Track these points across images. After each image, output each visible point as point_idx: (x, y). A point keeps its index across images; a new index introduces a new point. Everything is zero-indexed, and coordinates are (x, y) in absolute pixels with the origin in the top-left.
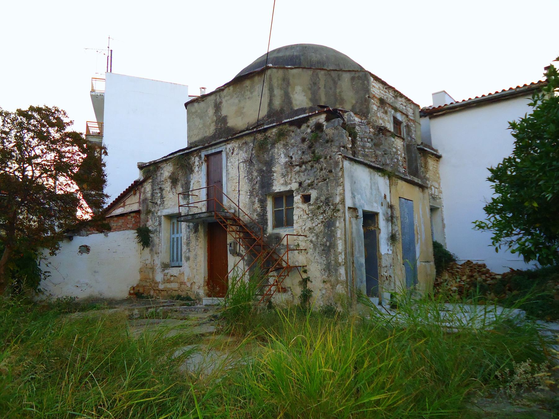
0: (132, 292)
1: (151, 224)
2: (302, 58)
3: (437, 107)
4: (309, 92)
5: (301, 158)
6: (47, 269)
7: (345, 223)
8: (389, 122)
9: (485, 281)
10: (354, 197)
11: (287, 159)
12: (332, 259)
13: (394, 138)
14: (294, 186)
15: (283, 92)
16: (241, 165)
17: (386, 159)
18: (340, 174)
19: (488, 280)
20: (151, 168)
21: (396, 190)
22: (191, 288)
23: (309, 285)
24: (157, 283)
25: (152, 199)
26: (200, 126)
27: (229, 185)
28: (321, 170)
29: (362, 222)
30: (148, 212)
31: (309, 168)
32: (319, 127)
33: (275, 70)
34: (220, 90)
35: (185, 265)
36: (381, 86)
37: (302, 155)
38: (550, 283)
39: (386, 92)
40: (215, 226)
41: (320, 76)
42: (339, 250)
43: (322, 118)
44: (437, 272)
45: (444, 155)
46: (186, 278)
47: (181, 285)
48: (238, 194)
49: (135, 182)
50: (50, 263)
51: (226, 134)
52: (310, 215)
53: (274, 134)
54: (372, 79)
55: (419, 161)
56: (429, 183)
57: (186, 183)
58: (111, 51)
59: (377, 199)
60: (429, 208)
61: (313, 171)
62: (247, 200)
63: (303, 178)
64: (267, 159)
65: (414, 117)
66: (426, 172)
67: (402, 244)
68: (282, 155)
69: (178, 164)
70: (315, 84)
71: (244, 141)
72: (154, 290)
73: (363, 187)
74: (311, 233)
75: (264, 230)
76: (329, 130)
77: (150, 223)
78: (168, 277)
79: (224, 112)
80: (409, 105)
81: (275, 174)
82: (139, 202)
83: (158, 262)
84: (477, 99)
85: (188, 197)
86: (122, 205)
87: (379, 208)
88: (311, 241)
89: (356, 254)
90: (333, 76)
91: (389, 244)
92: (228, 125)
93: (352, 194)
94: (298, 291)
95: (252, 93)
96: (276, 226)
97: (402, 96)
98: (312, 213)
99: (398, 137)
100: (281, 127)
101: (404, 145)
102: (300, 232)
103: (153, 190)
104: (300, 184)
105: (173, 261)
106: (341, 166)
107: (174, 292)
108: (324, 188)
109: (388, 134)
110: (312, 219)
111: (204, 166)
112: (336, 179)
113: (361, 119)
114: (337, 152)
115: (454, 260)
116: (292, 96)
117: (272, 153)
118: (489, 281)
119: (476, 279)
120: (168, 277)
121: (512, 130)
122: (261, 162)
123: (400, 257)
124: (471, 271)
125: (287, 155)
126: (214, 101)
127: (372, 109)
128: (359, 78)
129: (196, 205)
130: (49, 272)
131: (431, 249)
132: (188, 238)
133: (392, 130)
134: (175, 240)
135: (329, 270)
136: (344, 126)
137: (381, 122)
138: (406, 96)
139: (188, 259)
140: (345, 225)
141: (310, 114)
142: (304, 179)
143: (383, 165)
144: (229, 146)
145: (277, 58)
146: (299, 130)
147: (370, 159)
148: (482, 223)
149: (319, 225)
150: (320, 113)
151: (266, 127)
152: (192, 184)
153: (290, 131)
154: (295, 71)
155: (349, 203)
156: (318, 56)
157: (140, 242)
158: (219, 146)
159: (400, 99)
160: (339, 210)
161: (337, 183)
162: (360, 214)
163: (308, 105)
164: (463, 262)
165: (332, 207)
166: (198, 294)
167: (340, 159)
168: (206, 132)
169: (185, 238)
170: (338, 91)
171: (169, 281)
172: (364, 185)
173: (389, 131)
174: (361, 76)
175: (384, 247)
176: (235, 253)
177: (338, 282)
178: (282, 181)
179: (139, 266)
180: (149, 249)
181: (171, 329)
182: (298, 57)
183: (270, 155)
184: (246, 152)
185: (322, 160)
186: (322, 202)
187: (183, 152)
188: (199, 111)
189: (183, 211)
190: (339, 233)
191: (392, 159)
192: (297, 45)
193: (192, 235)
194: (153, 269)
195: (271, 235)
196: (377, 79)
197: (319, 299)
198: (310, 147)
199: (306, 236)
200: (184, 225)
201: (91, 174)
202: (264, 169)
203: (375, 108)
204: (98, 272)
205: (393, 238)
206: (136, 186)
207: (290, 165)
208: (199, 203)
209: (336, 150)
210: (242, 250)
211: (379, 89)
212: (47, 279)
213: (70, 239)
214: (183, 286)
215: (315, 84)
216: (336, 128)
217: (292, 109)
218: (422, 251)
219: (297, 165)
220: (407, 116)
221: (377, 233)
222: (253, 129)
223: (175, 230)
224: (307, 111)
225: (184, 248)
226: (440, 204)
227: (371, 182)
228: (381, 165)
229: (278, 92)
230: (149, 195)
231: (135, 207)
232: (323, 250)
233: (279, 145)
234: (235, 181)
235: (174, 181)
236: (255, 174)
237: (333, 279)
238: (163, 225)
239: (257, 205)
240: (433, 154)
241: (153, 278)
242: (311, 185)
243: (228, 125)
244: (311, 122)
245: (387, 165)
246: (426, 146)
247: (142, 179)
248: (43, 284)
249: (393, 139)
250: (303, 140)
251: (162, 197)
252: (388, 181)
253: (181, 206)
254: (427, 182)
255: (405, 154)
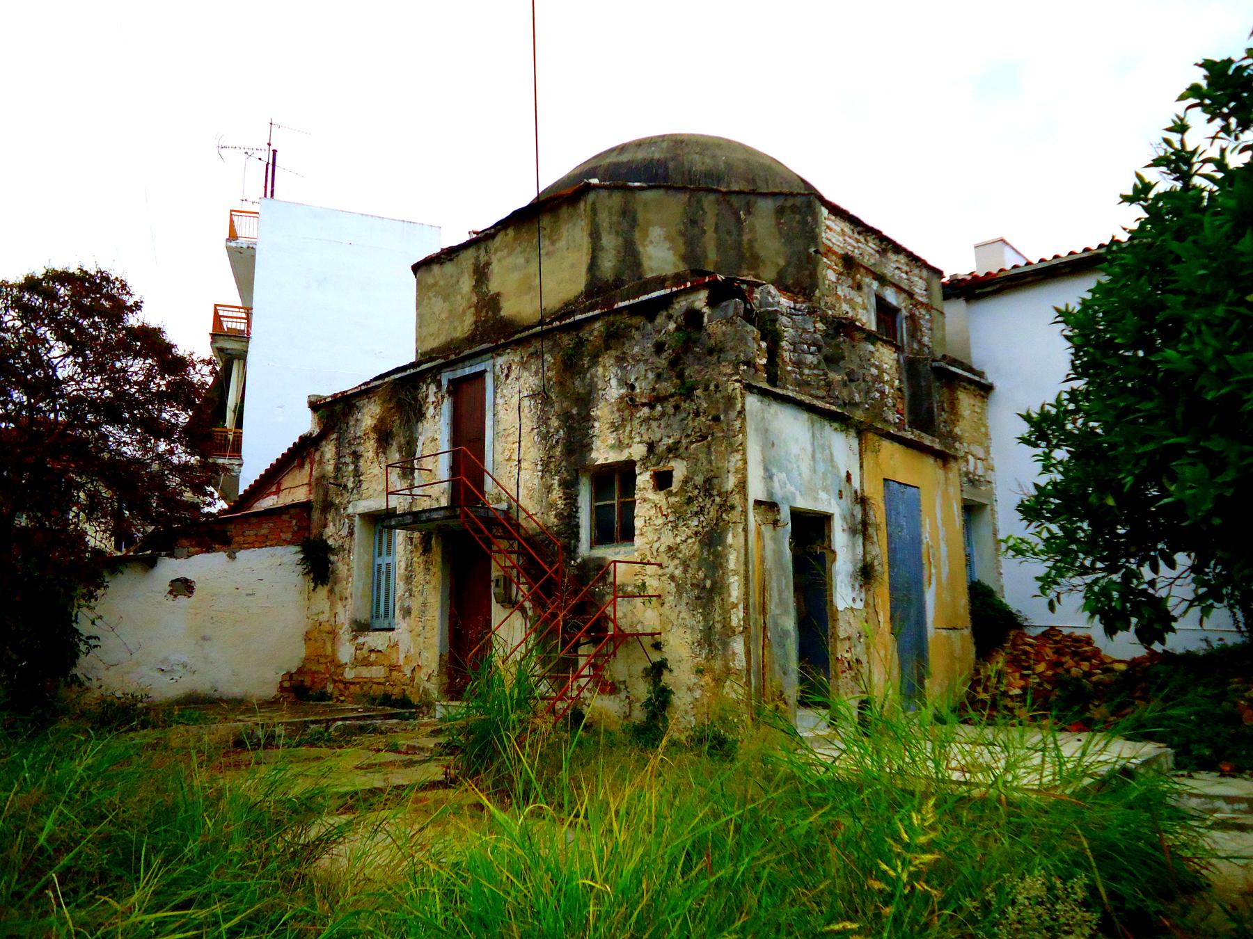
0: (286, 684)
1: (333, 533)
2: (671, 165)
3: (982, 274)
4: (681, 241)
5: (654, 389)
6: (94, 631)
7: (746, 536)
8: (865, 308)
9: (1088, 675)
10: (769, 477)
11: (623, 391)
12: (717, 618)
13: (873, 344)
14: (637, 451)
15: (620, 240)
16: (526, 403)
17: (851, 393)
18: (737, 424)
19: (1095, 674)
20: (338, 408)
21: (877, 464)
22: (412, 679)
23: (666, 678)
24: (341, 666)
25: (336, 478)
26: (443, 316)
27: (499, 448)
28: (697, 414)
29: (788, 535)
30: (328, 506)
31: (671, 411)
32: (693, 317)
33: (604, 193)
34: (482, 239)
35: (402, 625)
36: (847, 228)
37: (656, 382)
38: (1235, 683)
39: (858, 241)
40: (466, 540)
41: (706, 205)
42: (733, 599)
43: (700, 300)
44: (977, 652)
45: (999, 385)
46: (402, 656)
47: (391, 671)
48: (517, 469)
49: (301, 438)
50: (100, 617)
51: (496, 333)
52: (671, 518)
53: (596, 333)
54: (825, 212)
55: (936, 397)
56: (961, 448)
57: (408, 443)
58: (275, 151)
59: (829, 482)
60: (960, 505)
61: (679, 417)
62: (536, 481)
63: (656, 433)
64: (581, 391)
65: (929, 296)
66: (954, 423)
67: (893, 588)
68: (614, 382)
69: (390, 400)
70: (693, 222)
71: (532, 350)
72: (335, 681)
73: (793, 457)
74: (673, 557)
75: (571, 551)
76: (714, 326)
77: (330, 530)
78: (365, 652)
79: (494, 286)
80: (916, 271)
81: (596, 424)
82: (309, 484)
83: (344, 617)
84: (1073, 257)
85: (412, 473)
86: (274, 489)
87: (833, 502)
88: (672, 578)
89: (773, 608)
90: (736, 205)
91: (857, 586)
92: (502, 313)
93: (766, 469)
94: (642, 690)
95: (553, 243)
96: (597, 541)
97: (898, 249)
98: (675, 513)
99: (885, 342)
100: (612, 318)
101: (898, 361)
102: (647, 557)
103: (339, 456)
104: (651, 447)
105: (377, 617)
106: (739, 406)
107: (375, 686)
108: (702, 456)
109: (858, 335)
110: (675, 527)
111: (446, 406)
112: (729, 437)
113: (796, 302)
114: (731, 375)
115: (1021, 627)
116: (641, 249)
117: (592, 378)
118: (1098, 676)
119: (1068, 671)
120: (365, 652)
121: (1063, 326)
122: (566, 398)
123: (884, 617)
124: (1058, 652)
125: (623, 382)
126: (473, 260)
127: (825, 277)
128: (794, 209)
129: (428, 490)
130: (96, 638)
131: (963, 600)
132: (409, 565)
133: (874, 328)
134: (384, 569)
135: (710, 645)
136: (749, 316)
137: (845, 307)
138: (910, 249)
139: (407, 612)
140: (746, 540)
141: (675, 289)
142: (659, 436)
143: (845, 404)
144: (500, 361)
145: (617, 165)
146: (649, 326)
147: (813, 392)
148: (1023, 541)
149: (690, 541)
150: (695, 289)
151: (578, 317)
152: (420, 444)
153: (631, 326)
154: (650, 195)
155: (756, 491)
156: (708, 160)
157: (308, 573)
158: (479, 360)
159: (892, 256)
160: (732, 508)
161: (731, 445)
162: (785, 515)
163: (681, 270)
164: (1039, 631)
165: (718, 499)
166: (426, 692)
167: (738, 391)
168: (455, 328)
169: (403, 565)
170: (746, 238)
171: (366, 663)
172: (795, 449)
173: (861, 329)
174: (800, 203)
175: (844, 594)
176: (508, 602)
177: (728, 671)
178: (611, 439)
179: (302, 629)
180: (327, 588)
181: (347, 770)
182: (662, 164)
183: (587, 381)
184: (536, 373)
185: (699, 392)
186: (696, 487)
187: (403, 374)
188: (441, 283)
189: (399, 503)
190: (733, 561)
191: (867, 393)
192: (663, 138)
193: (418, 559)
194: (333, 633)
195: (585, 562)
196: (836, 211)
197: (686, 712)
198: (673, 364)
199: (660, 565)
200: (400, 536)
201: (211, 417)
202: (574, 411)
203: (832, 276)
204: (209, 639)
205: (866, 574)
206: (303, 450)
207: (629, 403)
208: (434, 485)
209: (728, 371)
210: (521, 591)
211: (843, 233)
212: (92, 653)
213: (150, 563)
214: (394, 673)
215: (693, 222)
216: (730, 321)
217: (640, 278)
218: (941, 601)
219: (644, 405)
220: (911, 295)
221: (828, 559)
222: (551, 322)
223: (382, 546)
224: (668, 283)
225: (400, 588)
226: (990, 494)
227: (813, 444)
228: (839, 406)
229: (610, 242)
230: (330, 468)
231: (301, 495)
232: (698, 598)
233: (607, 360)
234: (510, 439)
235: (384, 437)
236: (555, 423)
237: (718, 664)
238: (356, 536)
239: (557, 493)
240: (970, 381)
241: (334, 651)
242: (673, 450)
243: (502, 313)
244: (677, 306)
245: (856, 405)
246: (954, 362)
247: (317, 431)
248: (85, 665)
249: (871, 348)
250: (659, 348)
251: (357, 473)
252: (855, 443)
253: (392, 493)
254: (957, 445)
255: (900, 381)
